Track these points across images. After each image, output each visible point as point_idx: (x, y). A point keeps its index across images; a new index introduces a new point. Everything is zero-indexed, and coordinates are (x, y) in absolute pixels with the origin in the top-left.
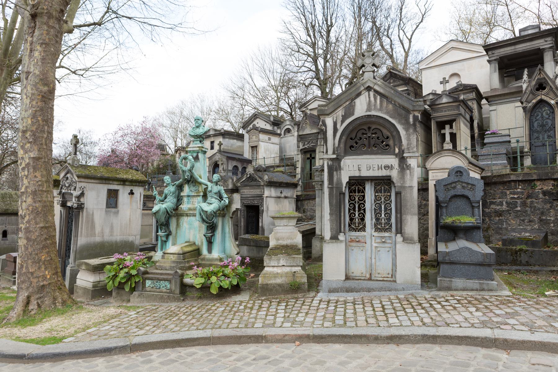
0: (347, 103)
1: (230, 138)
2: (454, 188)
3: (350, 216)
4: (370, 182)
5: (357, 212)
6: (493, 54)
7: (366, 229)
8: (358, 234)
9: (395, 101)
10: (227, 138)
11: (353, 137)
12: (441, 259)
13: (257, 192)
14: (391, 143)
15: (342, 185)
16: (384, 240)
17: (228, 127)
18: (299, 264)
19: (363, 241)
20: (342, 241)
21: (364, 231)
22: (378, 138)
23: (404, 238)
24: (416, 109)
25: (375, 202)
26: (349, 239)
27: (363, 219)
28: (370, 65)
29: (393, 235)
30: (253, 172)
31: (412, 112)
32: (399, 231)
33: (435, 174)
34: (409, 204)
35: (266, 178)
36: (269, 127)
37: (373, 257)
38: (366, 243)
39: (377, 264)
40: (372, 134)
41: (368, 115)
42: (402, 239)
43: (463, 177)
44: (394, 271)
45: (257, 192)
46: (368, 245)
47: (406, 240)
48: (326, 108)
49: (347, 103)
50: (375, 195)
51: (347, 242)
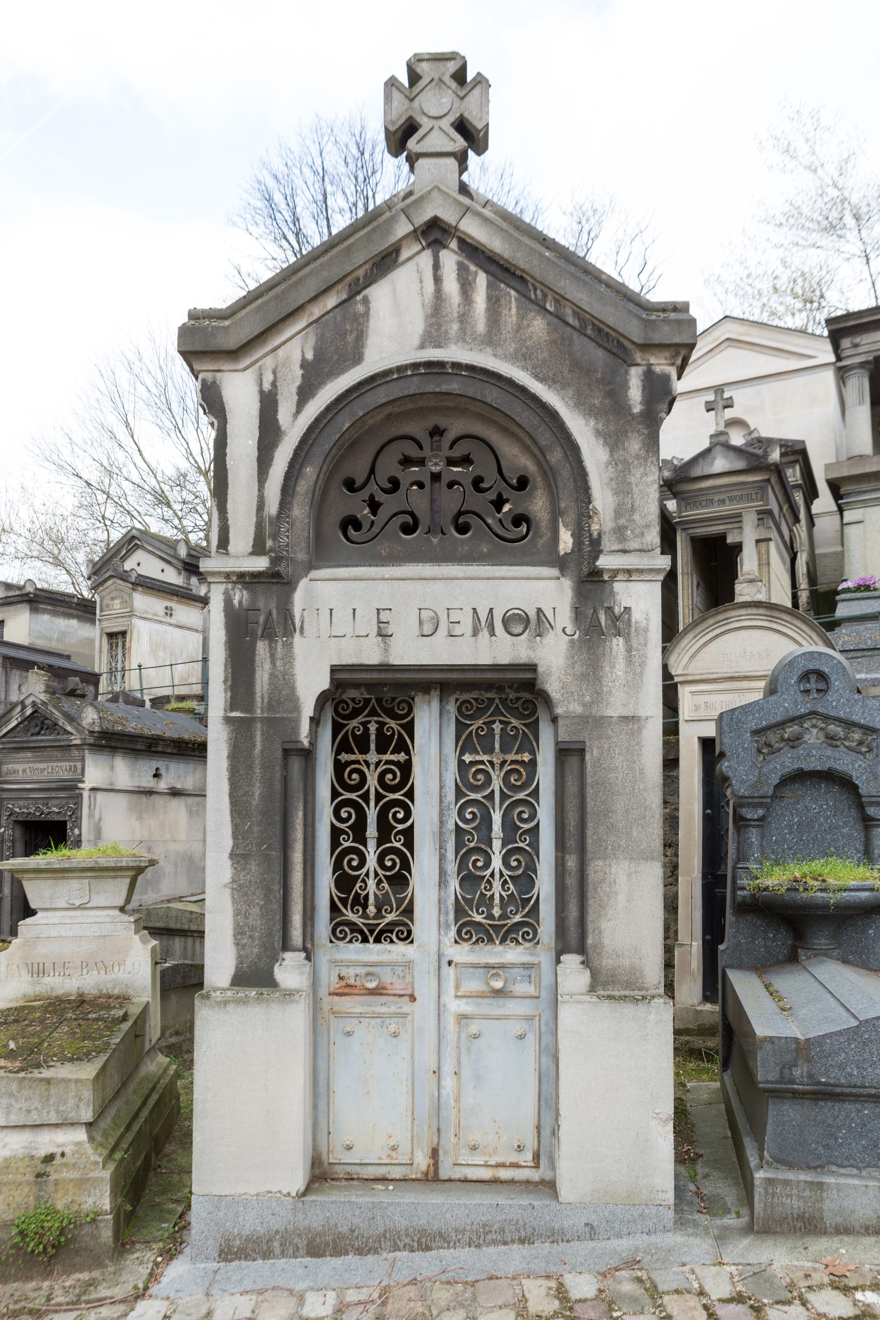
0: (331, 301)
1: (55, 614)
2: (794, 742)
4: (435, 695)
5: (372, 845)
6: (856, 346)
7: (417, 930)
8: (374, 952)
9: (560, 299)
10: (45, 611)
11: (358, 469)
12: (773, 1076)
13: (56, 770)
14: (538, 505)
15: (296, 708)
16: (498, 984)
17: (58, 581)
18: (72, 1116)
19: (398, 987)
20: (290, 995)
21: (407, 937)
22: (477, 482)
23: (594, 976)
24: (657, 338)
25: (459, 794)
26: (328, 978)
27: (400, 880)
28: (446, 123)
29: (544, 956)
30: (43, 697)
31: (638, 357)
32: (574, 938)
33: (702, 699)
34: (619, 805)
35: (89, 716)
36: (172, 576)
37: (448, 1068)
38: (413, 998)
39: (468, 1100)
40: (451, 462)
41: (429, 364)
42: (585, 978)
43: (831, 696)
44: (546, 1132)
45: (56, 770)
46: (423, 1011)
47: (606, 984)
48: (227, 323)
49: (331, 301)
50: (461, 763)
51: (323, 992)
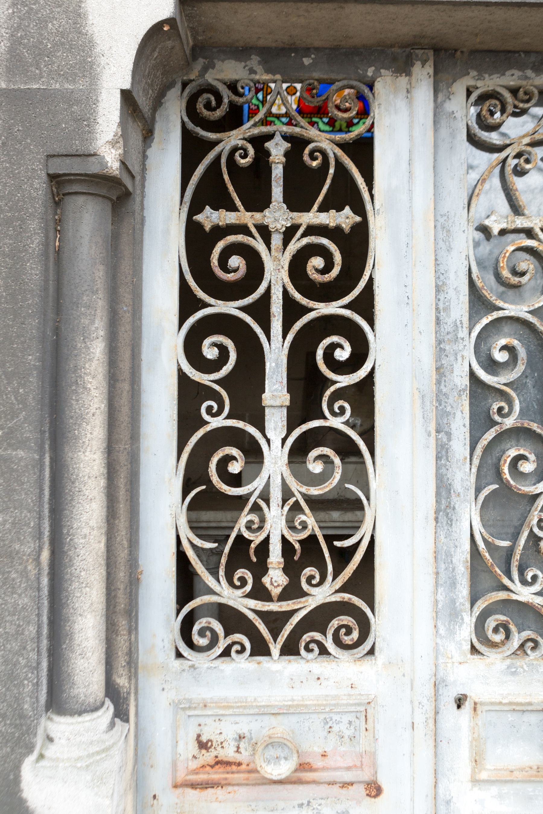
3: (193, 477)
4: (423, 75)
7: (381, 623)
8: (281, 678)
51: (159, 780)
